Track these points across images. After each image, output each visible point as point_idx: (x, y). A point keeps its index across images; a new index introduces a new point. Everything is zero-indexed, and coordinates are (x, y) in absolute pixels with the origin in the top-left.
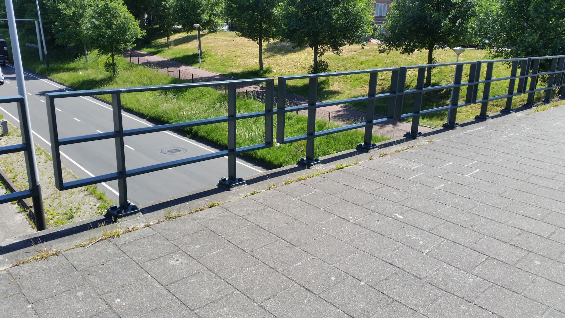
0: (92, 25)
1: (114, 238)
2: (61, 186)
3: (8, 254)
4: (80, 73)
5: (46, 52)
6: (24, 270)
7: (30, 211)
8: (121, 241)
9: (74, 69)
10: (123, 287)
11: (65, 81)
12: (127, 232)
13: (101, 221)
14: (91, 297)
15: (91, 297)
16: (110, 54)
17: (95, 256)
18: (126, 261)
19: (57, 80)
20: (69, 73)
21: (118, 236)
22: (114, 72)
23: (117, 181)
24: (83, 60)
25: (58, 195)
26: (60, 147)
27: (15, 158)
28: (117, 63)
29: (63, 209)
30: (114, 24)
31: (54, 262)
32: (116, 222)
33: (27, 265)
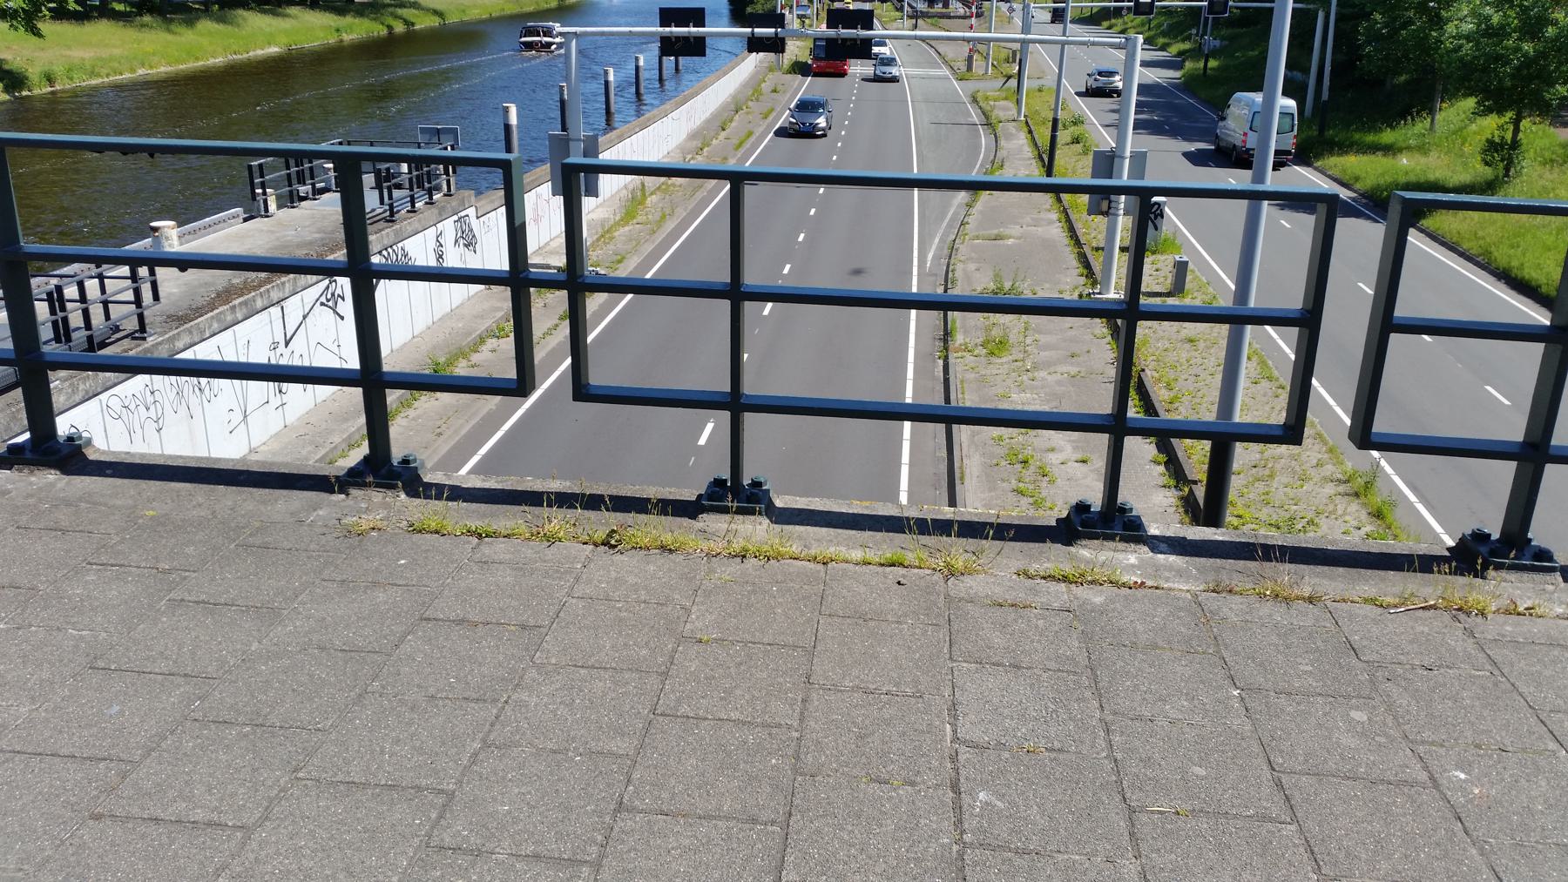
0: (1479, 25)
1: (1468, 614)
2: (1363, 436)
3: (1197, 559)
4: (1404, 161)
5: (1325, 96)
6: (1231, 608)
7: (1191, 491)
8: (1493, 627)
9: (1389, 150)
10: (1478, 747)
11: (1357, 179)
12: (1508, 612)
13: (1439, 560)
14: (1386, 735)
15: (1386, 735)
16: (1510, 115)
17: (1412, 642)
18: (1496, 684)
19: (1335, 172)
20: (1372, 157)
21: (1482, 613)
22: (1507, 169)
23: (1514, 464)
24: (1421, 126)
25: (1267, 472)
26: (1393, 336)
27: (1184, 355)
28: (1524, 141)
29: (1271, 510)
30: (1555, 23)
31: (1306, 616)
32: (1484, 578)
33: (1237, 598)
